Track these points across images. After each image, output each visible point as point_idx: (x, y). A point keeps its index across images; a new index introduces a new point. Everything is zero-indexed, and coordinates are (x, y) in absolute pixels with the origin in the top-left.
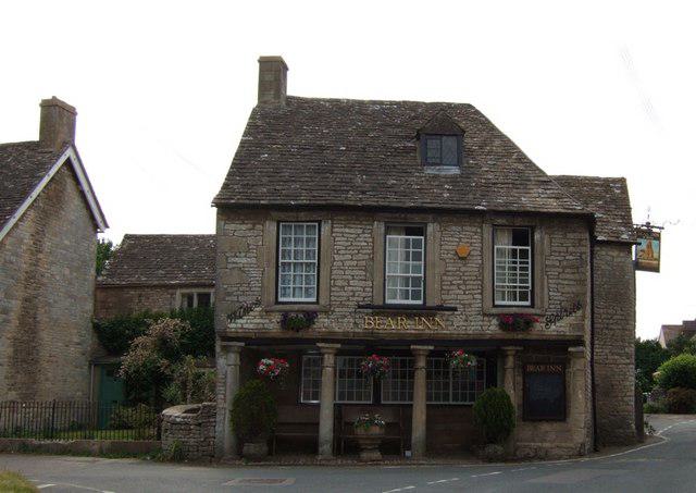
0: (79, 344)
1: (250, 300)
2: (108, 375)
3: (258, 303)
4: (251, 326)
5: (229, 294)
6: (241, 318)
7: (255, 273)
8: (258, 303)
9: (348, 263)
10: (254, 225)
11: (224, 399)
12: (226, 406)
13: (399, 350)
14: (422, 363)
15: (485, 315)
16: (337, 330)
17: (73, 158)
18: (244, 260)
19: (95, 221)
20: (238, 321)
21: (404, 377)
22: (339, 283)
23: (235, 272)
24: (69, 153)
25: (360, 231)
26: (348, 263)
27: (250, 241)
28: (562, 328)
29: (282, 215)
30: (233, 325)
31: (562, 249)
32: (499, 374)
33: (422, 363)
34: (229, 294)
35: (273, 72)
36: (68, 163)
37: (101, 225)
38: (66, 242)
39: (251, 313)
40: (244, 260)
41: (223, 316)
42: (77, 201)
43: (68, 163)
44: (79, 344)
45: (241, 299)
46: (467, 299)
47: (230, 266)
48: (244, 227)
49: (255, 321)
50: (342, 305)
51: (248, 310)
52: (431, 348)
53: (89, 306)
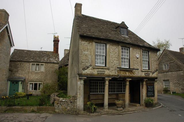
0: (5, 75)
1: (88, 65)
2: (12, 83)
3: (91, 65)
4: (89, 72)
5: (83, 62)
6: (86, 70)
7: (90, 57)
8: (91, 65)
9: (113, 56)
10: (89, 43)
11: (80, 94)
12: (80, 96)
13: (124, 79)
14: (107, 83)
15: (142, 71)
16: (111, 74)
17: (8, 26)
18: (87, 53)
19: (11, 44)
20: (85, 71)
21: (95, 86)
22: (111, 61)
23: (84, 56)
24: (7, 25)
25: (116, 48)
26: (113, 56)
27: (89, 47)
28: (155, 75)
29: (97, 41)
30: (84, 72)
31: (154, 57)
32: (141, 86)
33: (107, 83)
34: (83, 62)
35: (78, 6)
36: (7, 27)
37: (13, 45)
38: (5, 48)
39: (89, 68)
40: (87, 53)
41: (81, 69)
42: (7, 38)
43: (7, 27)
44: (5, 75)
45: (86, 64)
46: (138, 67)
47: (83, 54)
48: (87, 43)
49: (90, 71)
50: (112, 67)
51: (88, 67)
52: (131, 79)
53: (8, 65)
